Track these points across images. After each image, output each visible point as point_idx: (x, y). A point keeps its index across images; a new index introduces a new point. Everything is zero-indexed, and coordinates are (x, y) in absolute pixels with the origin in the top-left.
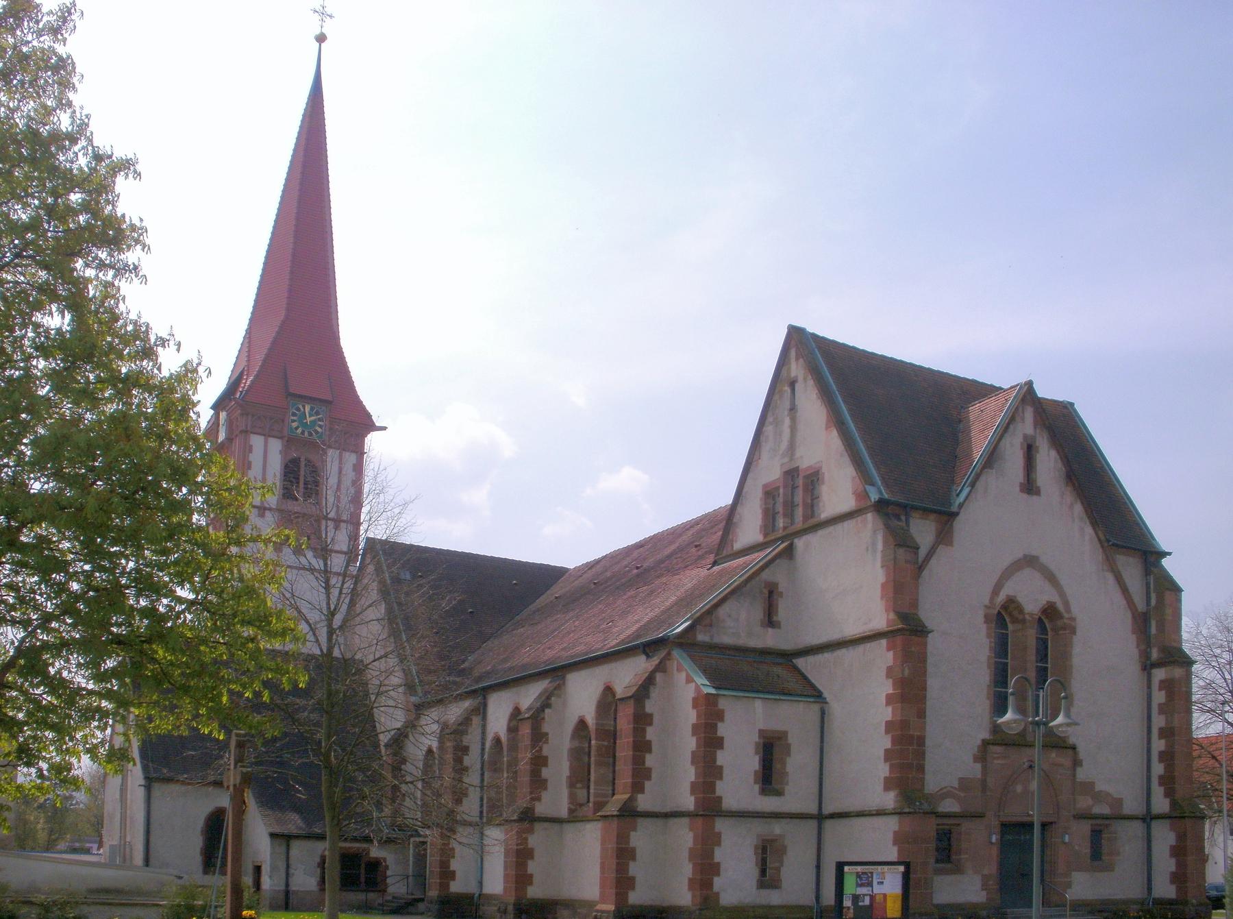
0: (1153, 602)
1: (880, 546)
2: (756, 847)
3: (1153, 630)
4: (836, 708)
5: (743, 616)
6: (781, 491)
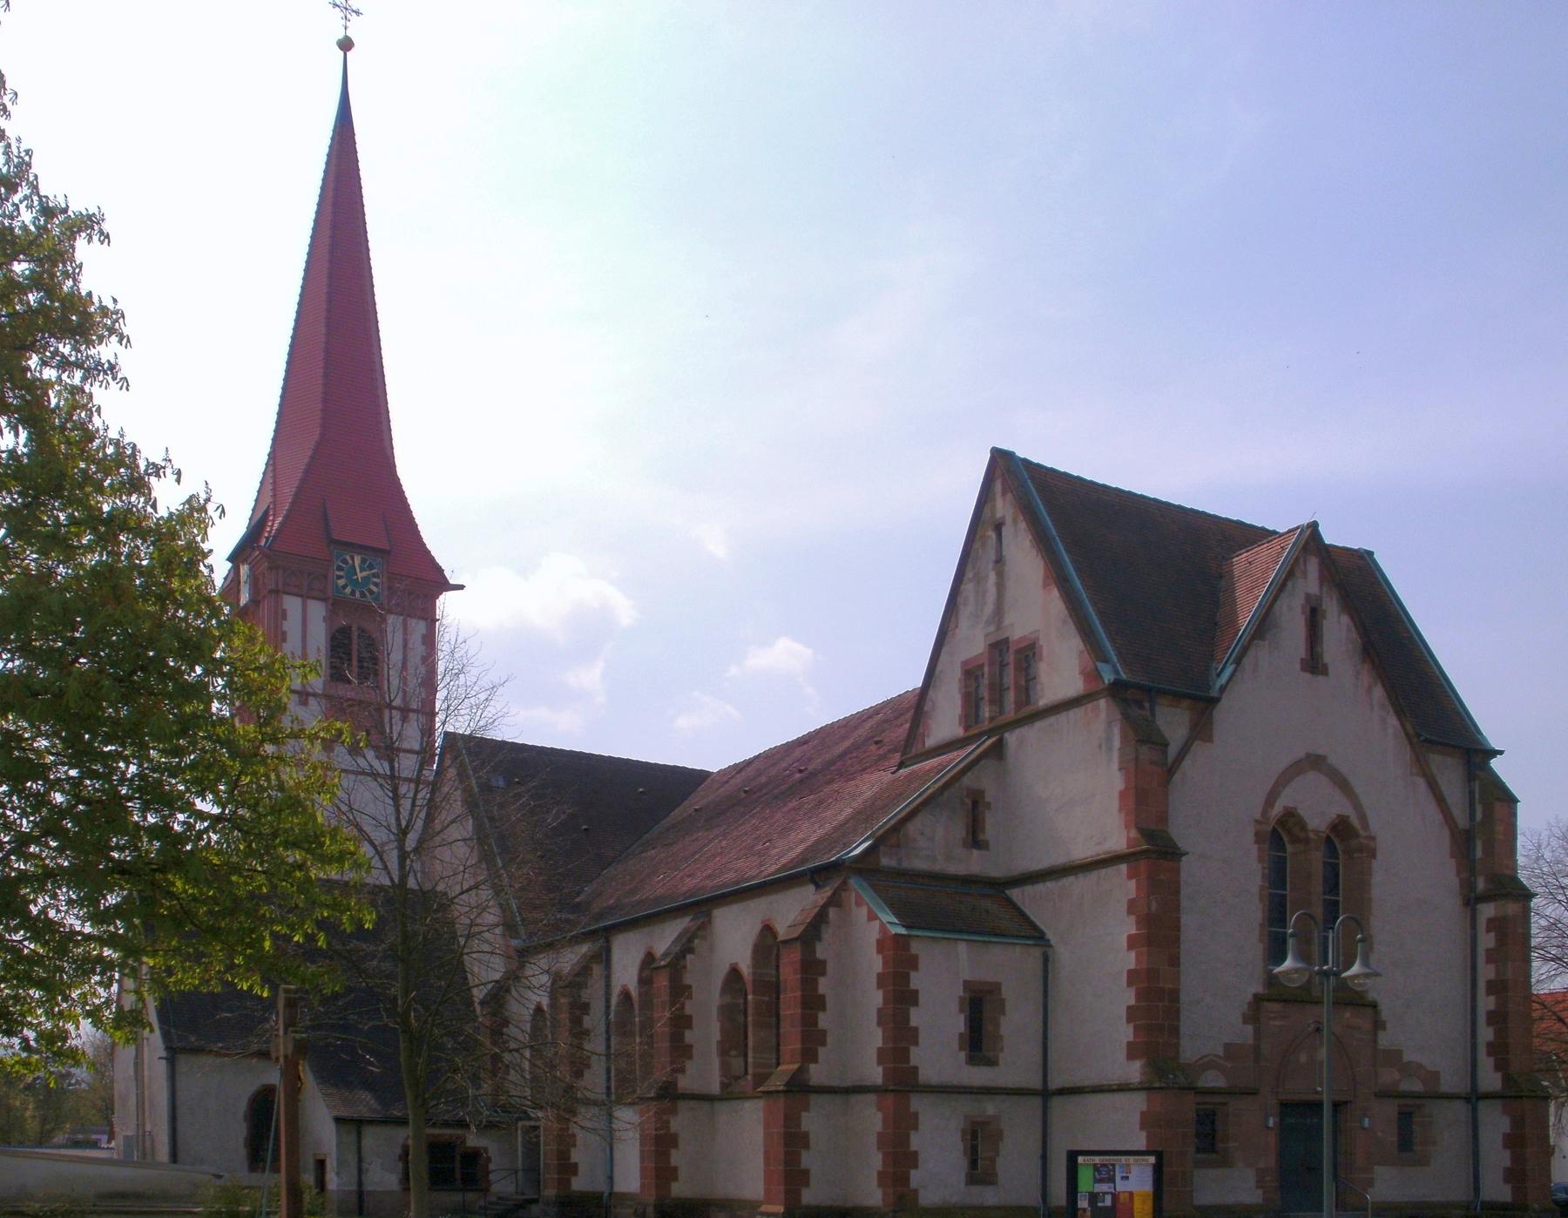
0: (1479, 816)
1: (1117, 743)
2: (964, 1132)
3: (1479, 853)
4: (1063, 954)
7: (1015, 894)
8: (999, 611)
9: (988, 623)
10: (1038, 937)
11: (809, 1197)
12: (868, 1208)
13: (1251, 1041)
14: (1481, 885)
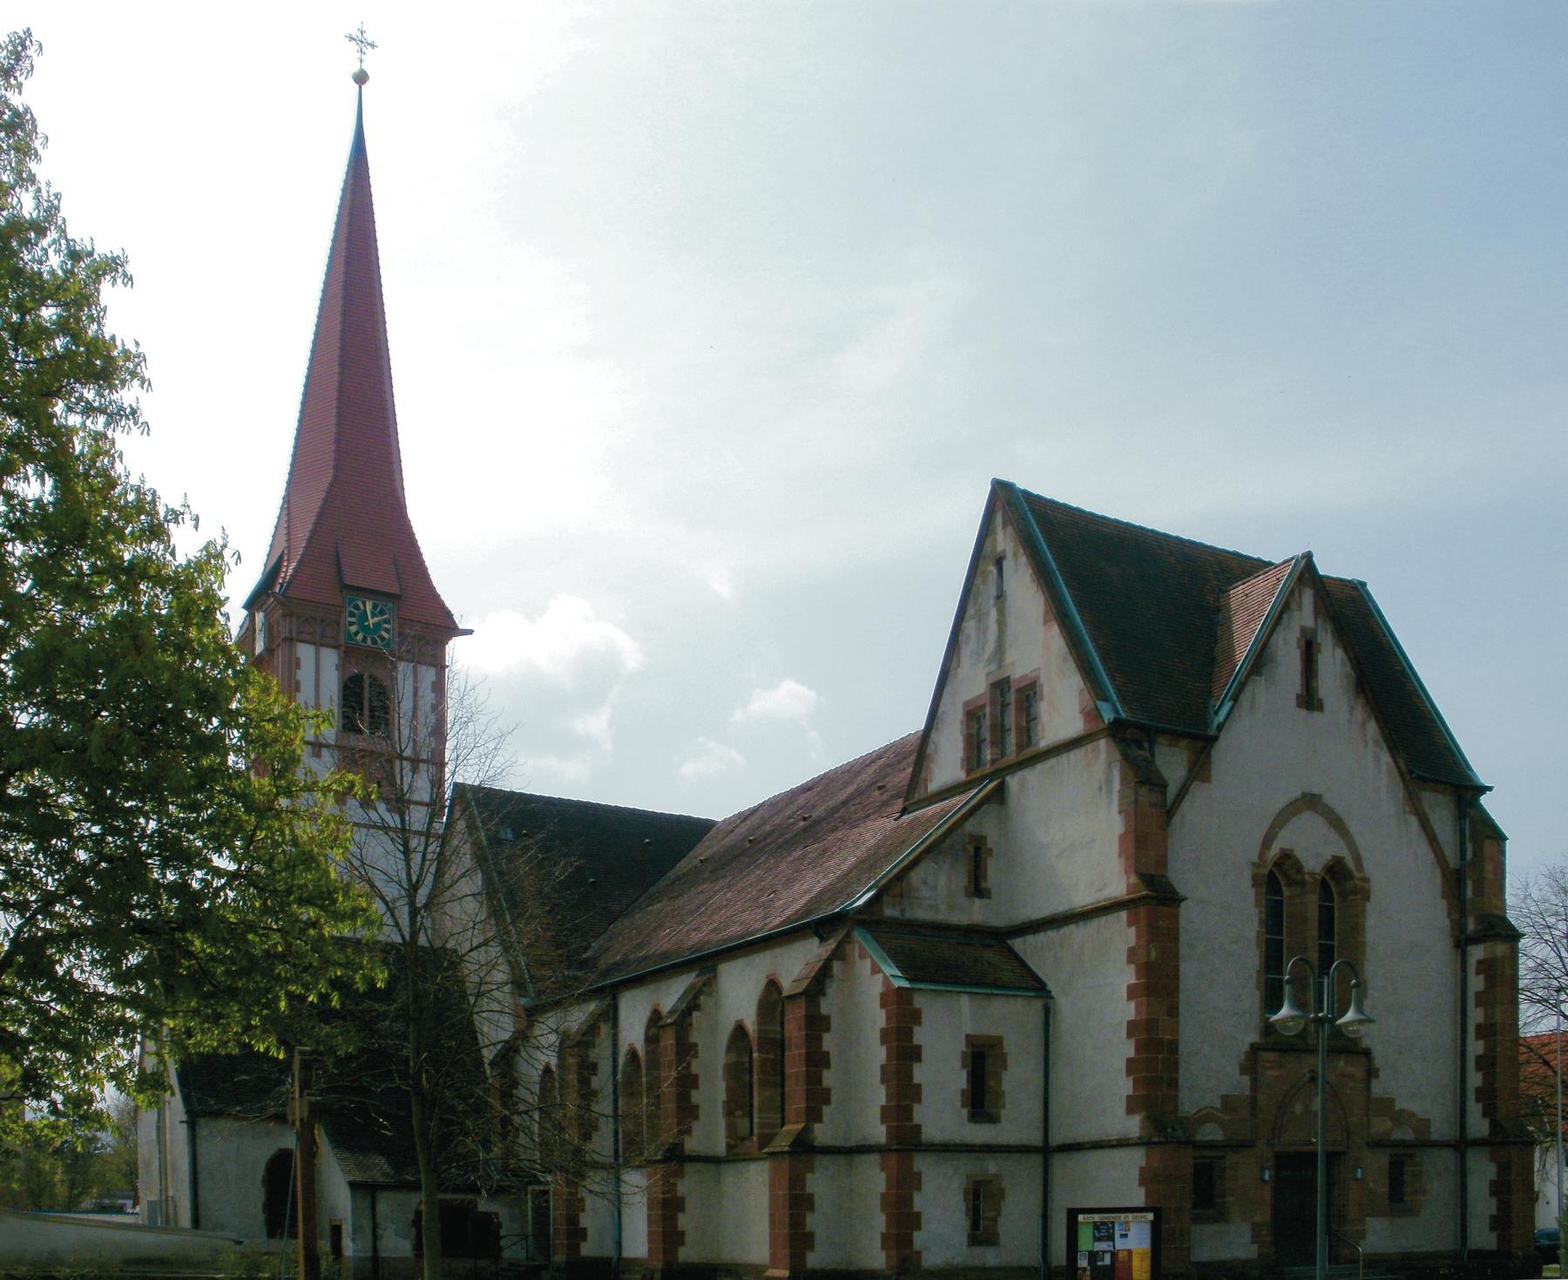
1: (1117, 785)
2: (966, 1192)
3: (1469, 893)
4: (1064, 1004)
6: (988, 710)
9: (990, 662)
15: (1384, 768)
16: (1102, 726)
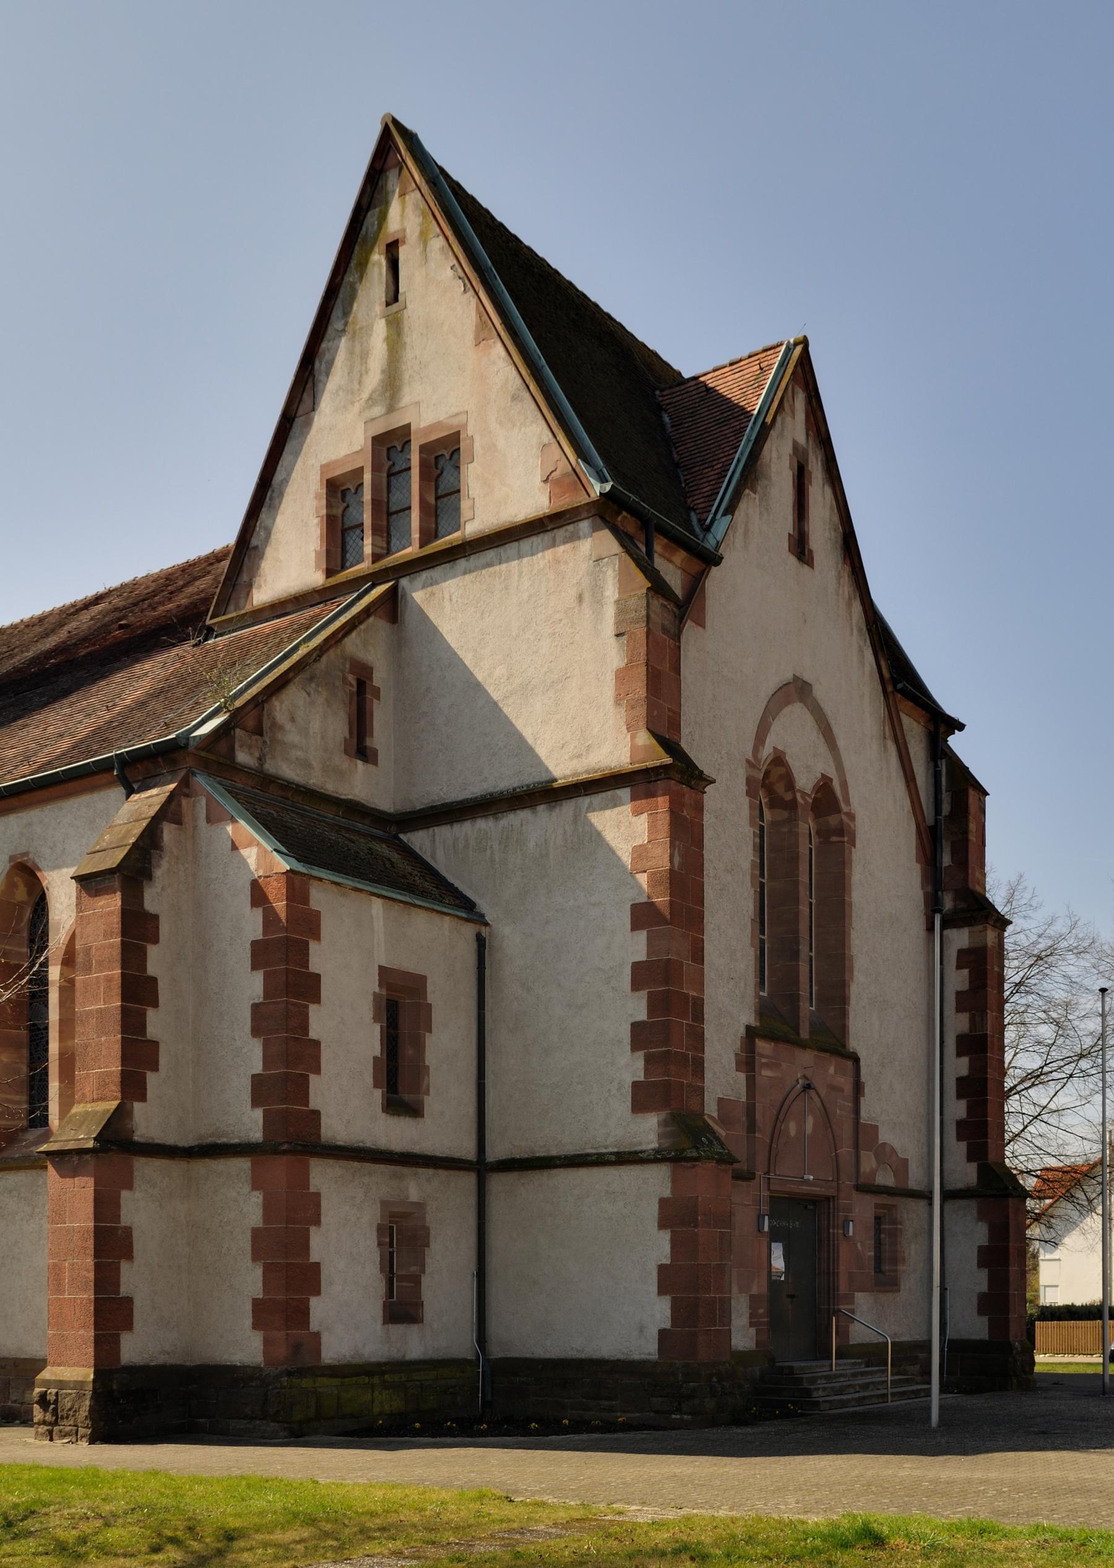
0: (946, 808)
1: (611, 592)
2: (380, 1229)
3: (946, 860)
4: (510, 938)
5: (315, 726)
6: (367, 477)
7: (418, 840)
8: (392, 384)
9: (371, 401)
10: (465, 907)
11: (134, 1349)
12: (231, 1369)
13: (744, 1099)
14: (948, 903)
15: (867, 669)
16: (583, 499)
